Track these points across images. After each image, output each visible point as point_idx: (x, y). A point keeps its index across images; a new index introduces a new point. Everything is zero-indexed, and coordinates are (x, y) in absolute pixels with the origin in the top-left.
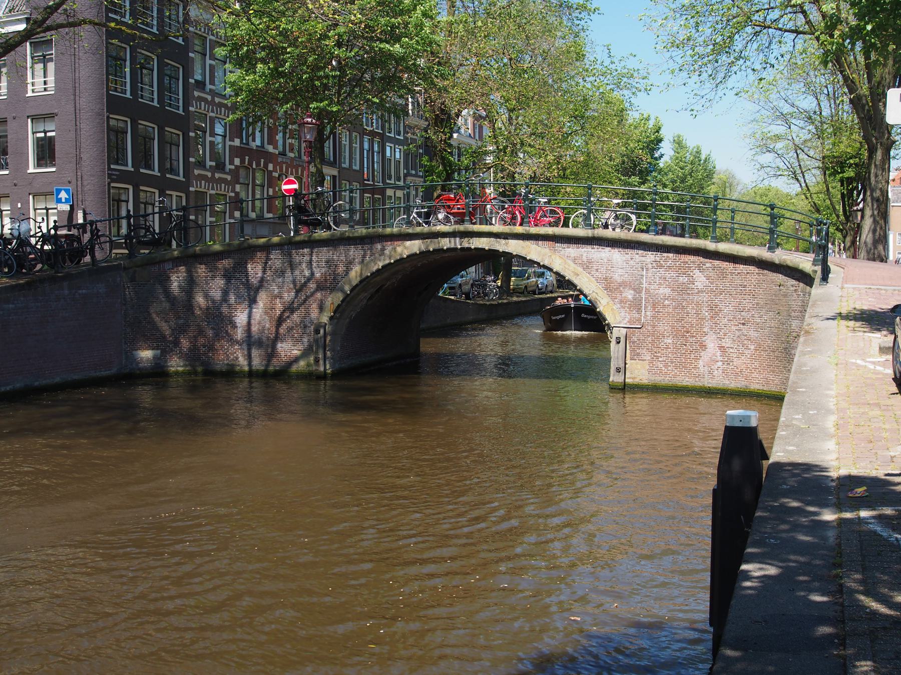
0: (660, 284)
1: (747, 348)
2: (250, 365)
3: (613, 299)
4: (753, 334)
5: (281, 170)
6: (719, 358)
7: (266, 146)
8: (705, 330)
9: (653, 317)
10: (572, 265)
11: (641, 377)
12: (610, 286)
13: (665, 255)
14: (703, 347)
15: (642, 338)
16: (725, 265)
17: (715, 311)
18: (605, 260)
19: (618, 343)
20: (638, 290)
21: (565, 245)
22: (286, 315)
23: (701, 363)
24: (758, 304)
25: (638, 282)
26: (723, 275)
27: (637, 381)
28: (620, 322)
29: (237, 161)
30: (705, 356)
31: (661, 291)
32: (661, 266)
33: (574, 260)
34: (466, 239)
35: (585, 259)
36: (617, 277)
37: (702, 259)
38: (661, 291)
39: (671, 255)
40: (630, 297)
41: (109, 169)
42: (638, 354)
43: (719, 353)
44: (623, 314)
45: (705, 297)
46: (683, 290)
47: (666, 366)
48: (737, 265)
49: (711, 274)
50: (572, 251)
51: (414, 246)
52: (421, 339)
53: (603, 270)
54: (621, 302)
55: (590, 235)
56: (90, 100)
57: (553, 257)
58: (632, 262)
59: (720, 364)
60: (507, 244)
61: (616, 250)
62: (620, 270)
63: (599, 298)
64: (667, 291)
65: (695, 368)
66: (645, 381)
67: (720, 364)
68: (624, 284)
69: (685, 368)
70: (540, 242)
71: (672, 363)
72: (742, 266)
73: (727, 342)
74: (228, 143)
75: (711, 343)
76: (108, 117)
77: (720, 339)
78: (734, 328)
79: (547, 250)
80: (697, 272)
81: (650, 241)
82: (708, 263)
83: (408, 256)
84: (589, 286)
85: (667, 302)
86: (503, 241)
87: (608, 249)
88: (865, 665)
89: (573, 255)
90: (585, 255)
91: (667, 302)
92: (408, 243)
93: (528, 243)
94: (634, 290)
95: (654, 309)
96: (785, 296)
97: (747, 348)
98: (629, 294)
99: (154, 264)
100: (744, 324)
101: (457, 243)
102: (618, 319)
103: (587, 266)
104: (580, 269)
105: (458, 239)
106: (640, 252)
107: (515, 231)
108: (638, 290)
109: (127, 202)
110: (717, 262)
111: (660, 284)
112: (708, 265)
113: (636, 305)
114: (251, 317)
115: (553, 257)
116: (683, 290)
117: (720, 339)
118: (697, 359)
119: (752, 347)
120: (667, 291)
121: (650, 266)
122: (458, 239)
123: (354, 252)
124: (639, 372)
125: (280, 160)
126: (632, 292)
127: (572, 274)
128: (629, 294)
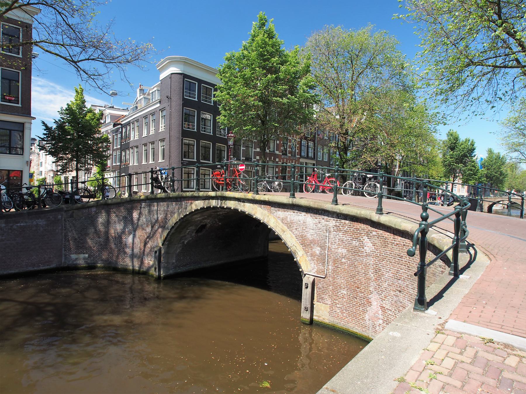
0: (339, 245)
2: (133, 266)
3: (307, 252)
5: (283, 161)
6: (381, 317)
7: (275, 151)
8: (371, 289)
10: (281, 224)
11: (324, 317)
12: (305, 243)
13: (343, 221)
14: (370, 303)
15: (325, 285)
16: (387, 235)
18: (302, 222)
19: (307, 288)
21: (277, 209)
22: (148, 240)
25: (323, 241)
27: (321, 319)
28: (310, 271)
29: (258, 158)
31: (340, 251)
33: (282, 220)
34: (224, 201)
35: (289, 220)
36: (309, 237)
37: (370, 228)
38: (340, 251)
39: (347, 222)
40: (318, 252)
41: (182, 160)
42: (322, 298)
43: (380, 312)
44: (312, 265)
46: (356, 252)
47: (342, 313)
48: (396, 237)
49: (376, 241)
50: (281, 213)
51: (198, 204)
52: (270, 244)
53: (300, 229)
54: (312, 255)
55: (291, 203)
56: (176, 133)
57: (270, 217)
58: (319, 225)
60: (244, 206)
61: (309, 215)
62: (311, 231)
63: (297, 251)
64: (344, 251)
65: (363, 319)
66: (327, 321)
67: (381, 322)
68: (313, 242)
69: (356, 318)
70: (262, 206)
71: (346, 311)
72: (400, 238)
74: (253, 150)
76: (182, 139)
77: (382, 300)
78: (392, 293)
80: (365, 238)
81: (330, 209)
82: (375, 232)
83: (195, 211)
84: (290, 240)
85: (343, 260)
86: (242, 204)
87: (304, 214)
88: (525, 193)
89: (281, 217)
90: (289, 217)
91: (343, 260)
92: (197, 202)
93: (256, 206)
94: (321, 247)
95: (335, 264)
98: (317, 250)
99: (86, 208)
100: (400, 291)
102: (310, 268)
103: (290, 225)
104: (285, 228)
105: (219, 201)
106: (326, 217)
107: (247, 197)
108: (323, 247)
109: (194, 174)
110: (381, 232)
112: (374, 233)
113: (322, 260)
114: (134, 241)
115: (270, 217)
117: (382, 300)
120: (344, 251)
121: (332, 229)
122: (219, 201)
123: (174, 206)
124: (323, 313)
125: (283, 157)
126: (319, 249)
127: (281, 231)
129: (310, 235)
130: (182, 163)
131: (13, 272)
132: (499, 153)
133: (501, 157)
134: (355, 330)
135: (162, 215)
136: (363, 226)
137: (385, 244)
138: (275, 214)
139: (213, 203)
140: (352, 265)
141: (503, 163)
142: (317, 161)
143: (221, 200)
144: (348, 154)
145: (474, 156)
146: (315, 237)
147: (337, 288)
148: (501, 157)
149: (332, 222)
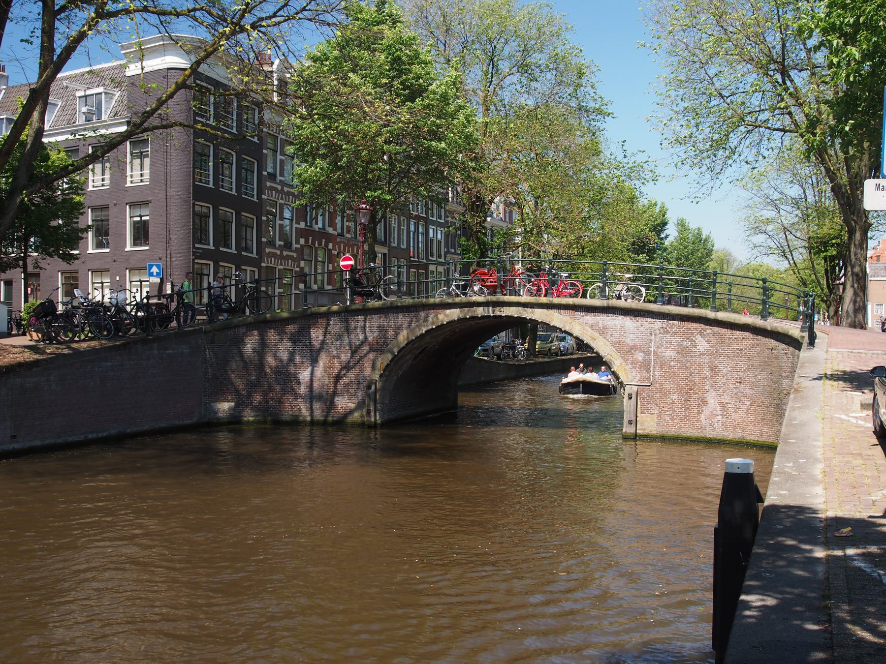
0: (667, 347)
1: (744, 404)
2: (312, 415)
3: (626, 360)
4: (748, 391)
5: (340, 248)
8: (707, 388)
9: (661, 376)
13: (671, 322)
14: (705, 403)
16: (723, 331)
17: (715, 372)
20: (647, 353)
21: (584, 314)
22: (344, 372)
23: (703, 417)
24: (752, 365)
26: (722, 340)
27: (647, 432)
28: (632, 381)
30: (707, 410)
32: (668, 332)
33: (592, 327)
35: (601, 325)
36: (628, 341)
37: (703, 326)
39: (676, 322)
40: (640, 359)
41: (194, 247)
42: (648, 409)
43: (718, 408)
44: (634, 373)
45: (706, 359)
46: (687, 353)
47: (672, 419)
50: (590, 318)
51: (454, 314)
53: (617, 335)
54: (633, 363)
56: (179, 189)
57: (573, 324)
58: (642, 329)
59: (720, 417)
60: (533, 312)
61: (628, 318)
66: (654, 432)
67: (720, 417)
68: (634, 347)
72: (738, 332)
73: (726, 399)
74: (295, 226)
75: (712, 400)
76: (194, 204)
77: (720, 396)
79: (568, 318)
80: (699, 337)
82: (709, 330)
85: (672, 363)
86: (530, 310)
93: (551, 312)
94: (644, 352)
96: (777, 358)
97: (744, 404)
98: (640, 356)
100: (740, 383)
101: (490, 312)
102: (630, 377)
103: (603, 332)
104: (597, 335)
106: (649, 320)
108: (647, 353)
109: (208, 275)
110: (716, 329)
111: (667, 347)
112: (708, 331)
113: (645, 366)
115: (573, 324)
116: (687, 353)
117: (720, 396)
118: (699, 413)
119: (748, 403)
121: (658, 332)
123: (402, 319)
124: (648, 424)
125: (338, 240)
128: (640, 356)
129: (629, 341)
130: (194, 253)
131: (163, 425)
132: (699, 229)
133: (704, 237)
134: (689, 435)
135: (376, 334)
136: (695, 325)
137: (722, 340)
138: (581, 320)
139: (480, 311)
140: (683, 367)
141: (709, 253)
142: (391, 248)
143: (494, 307)
144: (39, 199)
145: (666, 237)
146: (637, 342)
147: (665, 394)
148: (704, 237)
149: (658, 324)
